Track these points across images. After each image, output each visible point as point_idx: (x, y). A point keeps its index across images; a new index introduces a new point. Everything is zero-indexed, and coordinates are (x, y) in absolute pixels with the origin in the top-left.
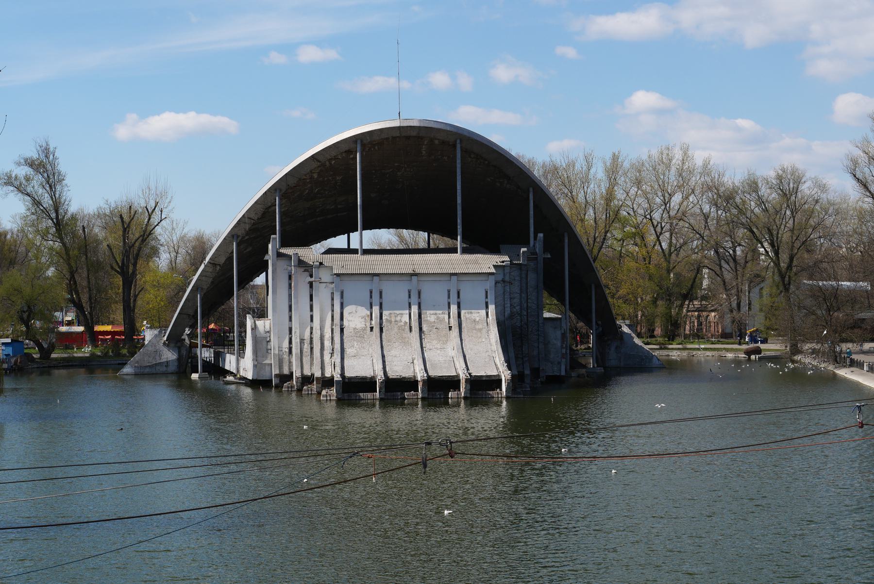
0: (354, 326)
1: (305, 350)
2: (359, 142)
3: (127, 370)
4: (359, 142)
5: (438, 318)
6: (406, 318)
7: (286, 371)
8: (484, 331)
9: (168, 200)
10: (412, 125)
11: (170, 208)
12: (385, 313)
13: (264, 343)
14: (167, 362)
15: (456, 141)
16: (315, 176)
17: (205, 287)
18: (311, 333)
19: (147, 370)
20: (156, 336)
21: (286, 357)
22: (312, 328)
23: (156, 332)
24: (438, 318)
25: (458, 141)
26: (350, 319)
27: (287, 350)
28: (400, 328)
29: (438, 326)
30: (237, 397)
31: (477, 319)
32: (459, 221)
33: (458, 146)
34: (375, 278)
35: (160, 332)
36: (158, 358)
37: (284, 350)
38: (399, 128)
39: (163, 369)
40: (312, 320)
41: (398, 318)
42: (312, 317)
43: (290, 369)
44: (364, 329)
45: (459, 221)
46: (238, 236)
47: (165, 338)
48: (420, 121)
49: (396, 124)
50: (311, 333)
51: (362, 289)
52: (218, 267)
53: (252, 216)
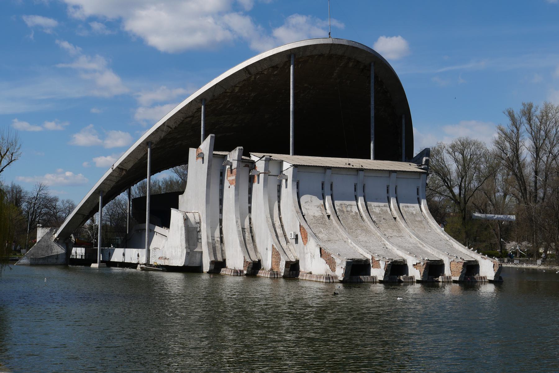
0: (312, 214)
1: (247, 238)
2: (292, 56)
3: (24, 261)
4: (292, 56)
5: (382, 210)
6: (355, 209)
7: (220, 259)
8: (424, 222)
9: (17, 147)
10: (342, 43)
11: (20, 151)
12: (336, 203)
13: (195, 233)
14: (57, 255)
15: (370, 65)
16: (237, 90)
17: (107, 190)
18: (250, 223)
19: (41, 262)
20: (47, 234)
21: (218, 245)
22: (250, 219)
23: (47, 230)
24: (382, 210)
25: (372, 64)
26: (307, 207)
27: (219, 239)
28: (353, 217)
29: (385, 217)
30: (162, 284)
31: (414, 213)
32: (372, 131)
33: (372, 69)
34: (328, 171)
35: (51, 230)
36: (50, 252)
37: (216, 239)
38: (332, 45)
39: (54, 261)
40: (250, 211)
41: (349, 209)
42: (250, 209)
43: (222, 257)
44: (323, 217)
45: (372, 131)
46: (152, 143)
47: (56, 235)
48: (348, 41)
49: (329, 41)
50: (250, 223)
51: (316, 180)
52: (124, 172)
53: (171, 125)
